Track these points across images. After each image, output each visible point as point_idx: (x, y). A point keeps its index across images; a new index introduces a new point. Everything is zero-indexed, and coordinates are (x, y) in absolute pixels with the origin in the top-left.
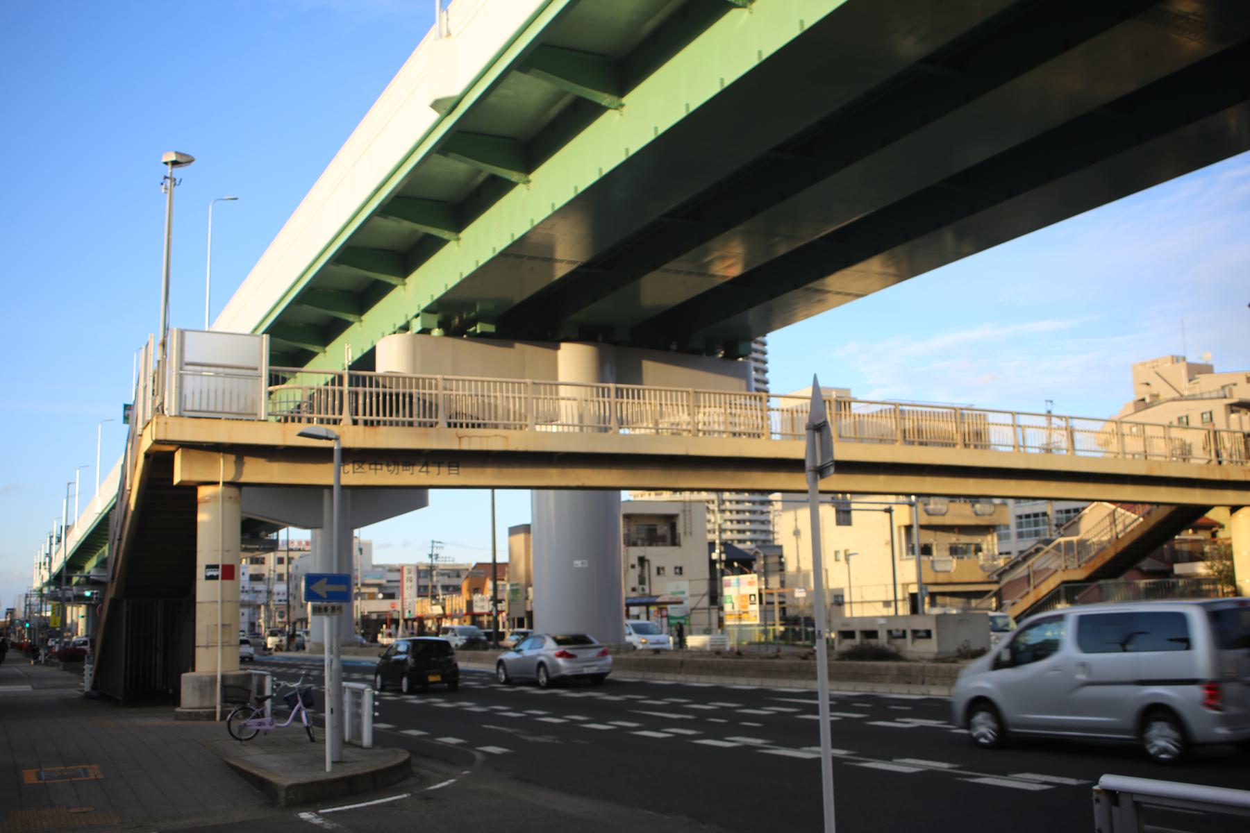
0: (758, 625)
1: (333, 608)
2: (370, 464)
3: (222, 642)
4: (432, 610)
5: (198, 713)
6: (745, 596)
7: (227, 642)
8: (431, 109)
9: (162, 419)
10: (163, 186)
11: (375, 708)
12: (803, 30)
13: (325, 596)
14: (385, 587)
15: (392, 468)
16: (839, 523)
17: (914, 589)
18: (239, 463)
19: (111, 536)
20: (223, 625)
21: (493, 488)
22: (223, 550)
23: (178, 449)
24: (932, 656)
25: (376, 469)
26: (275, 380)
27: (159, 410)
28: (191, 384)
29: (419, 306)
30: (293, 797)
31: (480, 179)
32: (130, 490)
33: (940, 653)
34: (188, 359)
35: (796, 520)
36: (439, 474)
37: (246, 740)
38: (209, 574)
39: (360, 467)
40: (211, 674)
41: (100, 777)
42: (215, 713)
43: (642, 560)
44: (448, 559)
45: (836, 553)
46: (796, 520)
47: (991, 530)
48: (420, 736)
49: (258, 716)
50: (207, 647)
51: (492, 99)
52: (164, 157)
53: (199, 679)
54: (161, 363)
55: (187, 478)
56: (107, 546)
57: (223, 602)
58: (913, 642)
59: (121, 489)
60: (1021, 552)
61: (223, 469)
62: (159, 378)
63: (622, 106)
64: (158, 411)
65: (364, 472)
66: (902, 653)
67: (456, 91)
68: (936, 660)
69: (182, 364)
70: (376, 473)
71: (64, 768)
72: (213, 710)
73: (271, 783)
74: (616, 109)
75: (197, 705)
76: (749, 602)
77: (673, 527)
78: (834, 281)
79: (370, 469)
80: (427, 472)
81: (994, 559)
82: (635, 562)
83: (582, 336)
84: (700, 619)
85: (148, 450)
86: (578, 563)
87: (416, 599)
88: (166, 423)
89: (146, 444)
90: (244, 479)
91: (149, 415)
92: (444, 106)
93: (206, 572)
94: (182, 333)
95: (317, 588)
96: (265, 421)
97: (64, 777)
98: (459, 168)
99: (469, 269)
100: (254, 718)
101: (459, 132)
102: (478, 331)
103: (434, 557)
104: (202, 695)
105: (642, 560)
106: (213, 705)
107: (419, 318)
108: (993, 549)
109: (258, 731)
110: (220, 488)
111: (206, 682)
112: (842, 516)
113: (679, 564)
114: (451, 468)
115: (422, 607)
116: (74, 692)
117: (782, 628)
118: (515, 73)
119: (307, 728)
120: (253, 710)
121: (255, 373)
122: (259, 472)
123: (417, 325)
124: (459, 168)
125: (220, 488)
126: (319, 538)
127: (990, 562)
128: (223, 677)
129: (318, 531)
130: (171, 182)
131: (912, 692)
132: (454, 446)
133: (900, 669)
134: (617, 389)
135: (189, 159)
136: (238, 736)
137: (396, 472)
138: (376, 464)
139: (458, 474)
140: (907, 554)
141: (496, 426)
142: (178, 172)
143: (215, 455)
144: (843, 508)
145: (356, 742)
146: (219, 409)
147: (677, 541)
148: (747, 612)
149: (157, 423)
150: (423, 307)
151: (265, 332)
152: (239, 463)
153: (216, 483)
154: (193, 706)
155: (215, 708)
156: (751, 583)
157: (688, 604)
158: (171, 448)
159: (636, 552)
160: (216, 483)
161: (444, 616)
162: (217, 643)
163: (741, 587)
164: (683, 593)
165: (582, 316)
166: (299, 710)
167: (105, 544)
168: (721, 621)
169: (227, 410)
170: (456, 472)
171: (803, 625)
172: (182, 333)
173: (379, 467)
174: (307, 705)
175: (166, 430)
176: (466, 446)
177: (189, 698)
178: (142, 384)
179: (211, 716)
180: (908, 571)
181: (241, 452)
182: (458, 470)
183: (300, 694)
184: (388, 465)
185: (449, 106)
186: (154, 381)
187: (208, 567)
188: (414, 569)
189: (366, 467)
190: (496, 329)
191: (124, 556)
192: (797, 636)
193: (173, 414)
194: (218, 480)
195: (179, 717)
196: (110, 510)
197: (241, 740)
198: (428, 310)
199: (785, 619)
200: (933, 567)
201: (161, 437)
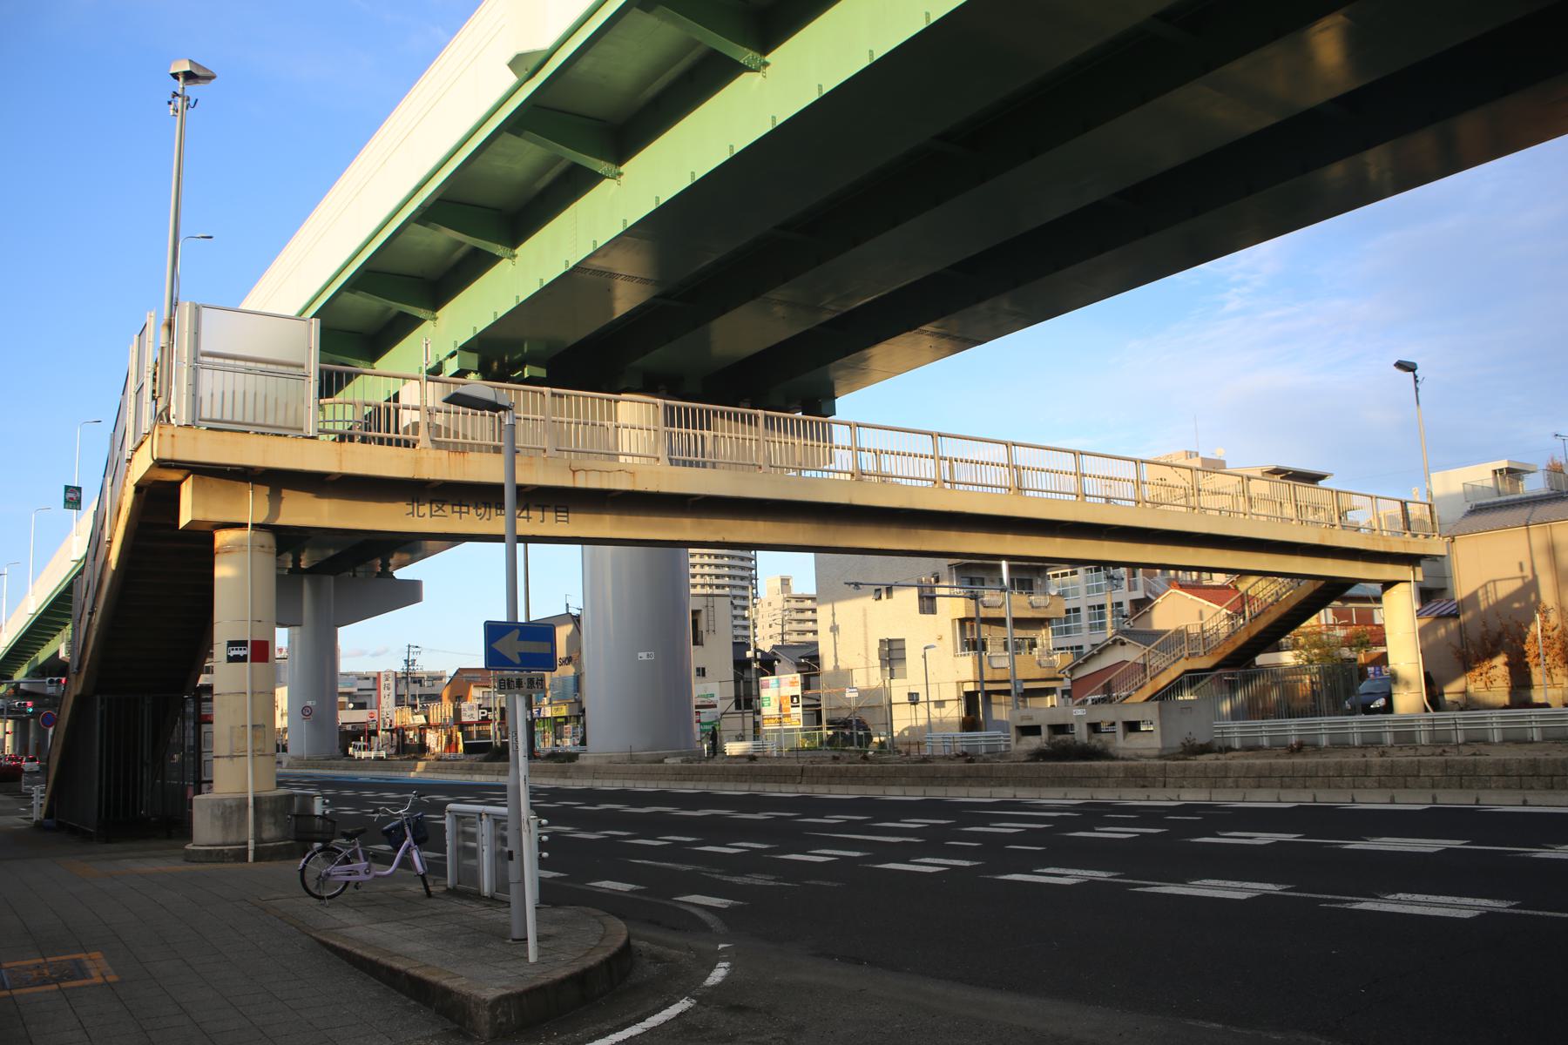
0: (801, 730)
1: (531, 681)
2: (453, 505)
3: (253, 751)
4: (413, 719)
5: (222, 850)
6: (786, 697)
7: (259, 750)
8: (508, 67)
9: (168, 431)
10: (172, 107)
11: (542, 846)
12: (821, 95)
13: (518, 661)
14: (356, 696)
15: (481, 511)
16: (922, 611)
17: (970, 687)
18: (275, 499)
19: (76, 611)
20: (254, 726)
22: (252, 621)
23: (186, 477)
24: (1156, 752)
25: (460, 512)
26: (330, 384)
27: (162, 417)
28: (211, 382)
29: (456, 342)
30: (504, 1020)
31: (463, 250)
32: (110, 542)
33: (1163, 749)
34: (204, 347)
35: (834, 615)
36: (542, 521)
37: (329, 898)
38: (232, 654)
39: (440, 509)
40: (238, 796)
41: (112, 978)
42: (246, 851)
46: (834, 615)
47: (1047, 623)
48: (554, 878)
49: (347, 861)
50: (231, 757)
51: (584, 65)
52: (172, 66)
53: (220, 803)
54: (166, 350)
55: (200, 517)
56: (69, 627)
57: (253, 693)
58: (1125, 736)
59: (93, 545)
60: (1094, 646)
61: (252, 506)
62: (161, 373)
63: (620, 174)
64: (162, 419)
66: (1111, 750)
67: (546, 44)
68: (1160, 757)
69: (198, 355)
70: (461, 518)
71: (42, 961)
72: (244, 847)
73: (447, 992)
74: (614, 178)
75: (219, 840)
76: (791, 704)
78: (879, 353)
79: (453, 512)
80: (528, 518)
81: (1049, 655)
83: (649, 386)
84: (733, 723)
85: (142, 479)
86: (643, 655)
87: (395, 708)
88: (173, 436)
89: (141, 466)
90: (281, 521)
91: (147, 423)
92: (525, 65)
93: (228, 651)
94: (197, 309)
95: (504, 645)
96: (312, 438)
97: (45, 983)
98: (442, 238)
99: (506, 306)
100: (340, 864)
101: (367, 271)
102: (526, 375)
104: (226, 826)
106: (243, 839)
107: (456, 357)
108: (1048, 644)
109: (347, 883)
110: (248, 532)
111: (231, 807)
112: (926, 602)
114: (558, 514)
115: (402, 717)
116: (15, 821)
117: (830, 733)
118: (506, 135)
119: (423, 877)
120: (340, 852)
121: (300, 371)
122: (302, 511)
123: (452, 366)
124: (442, 238)
125: (248, 532)
126: (297, 638)
127: (1045, 658)
128: (256, 799)
129: (297, 630)
130: (183, 100)
131: (1357, 800)
132: (566, 481)
133: (1126, 769)
134: (766, 417)
135: (209, 74)
136: (317, 893)
137: (487, 516)
138: (460, 505)
139: (568, 521)
140: (963, 650)
142: (193, 90)
143: (241, 485)
144: (927, 592)
145: (500, 895)
146: (249, 419)
147: (699, 639)
148: (789, 716)
149: (160, 435)
150: (459, 344)
151: (315, 316)
152: (275, 499)
153: (242, 526)
154: (212, 843)
155: (246, 843)
156: (793, 684)
157: (721, 708)
158: (174, 476)
160: (242, 526)
161: (428, 725)
162: (246, 751)
163: (782, 688)
164: (712, 696)
165: (659, 357)
166: (407, 851)
167: (66, 624)
168: (756, 725)
169: (260, 421)
170: (565, 519)
171: (855, 728)
172: (197, 309)
173: (464, 509)
174: (420, 841)
175: (173, 445)
177: (206, 830)
178: (132, 386)
179: (241, 856)
180: (965, 668)
181: (278, 481)
182: (567, 516)
183: (409, 825)
184: (477, 507)
185: (532, 66)
186: (154, 380)
187: (232, 644)
188: (391, 675)
189: (448, 508)
190: (547, 374)
191: (97, 635)
192: (848, 740)
193: (184, 423)
194: (244, 521)
195: (191, 857)
196: (76, 577)
197: (321, 898)
198: (467, 347)
199: (832, 723)
200: (990, 663)
201: (166, 455)
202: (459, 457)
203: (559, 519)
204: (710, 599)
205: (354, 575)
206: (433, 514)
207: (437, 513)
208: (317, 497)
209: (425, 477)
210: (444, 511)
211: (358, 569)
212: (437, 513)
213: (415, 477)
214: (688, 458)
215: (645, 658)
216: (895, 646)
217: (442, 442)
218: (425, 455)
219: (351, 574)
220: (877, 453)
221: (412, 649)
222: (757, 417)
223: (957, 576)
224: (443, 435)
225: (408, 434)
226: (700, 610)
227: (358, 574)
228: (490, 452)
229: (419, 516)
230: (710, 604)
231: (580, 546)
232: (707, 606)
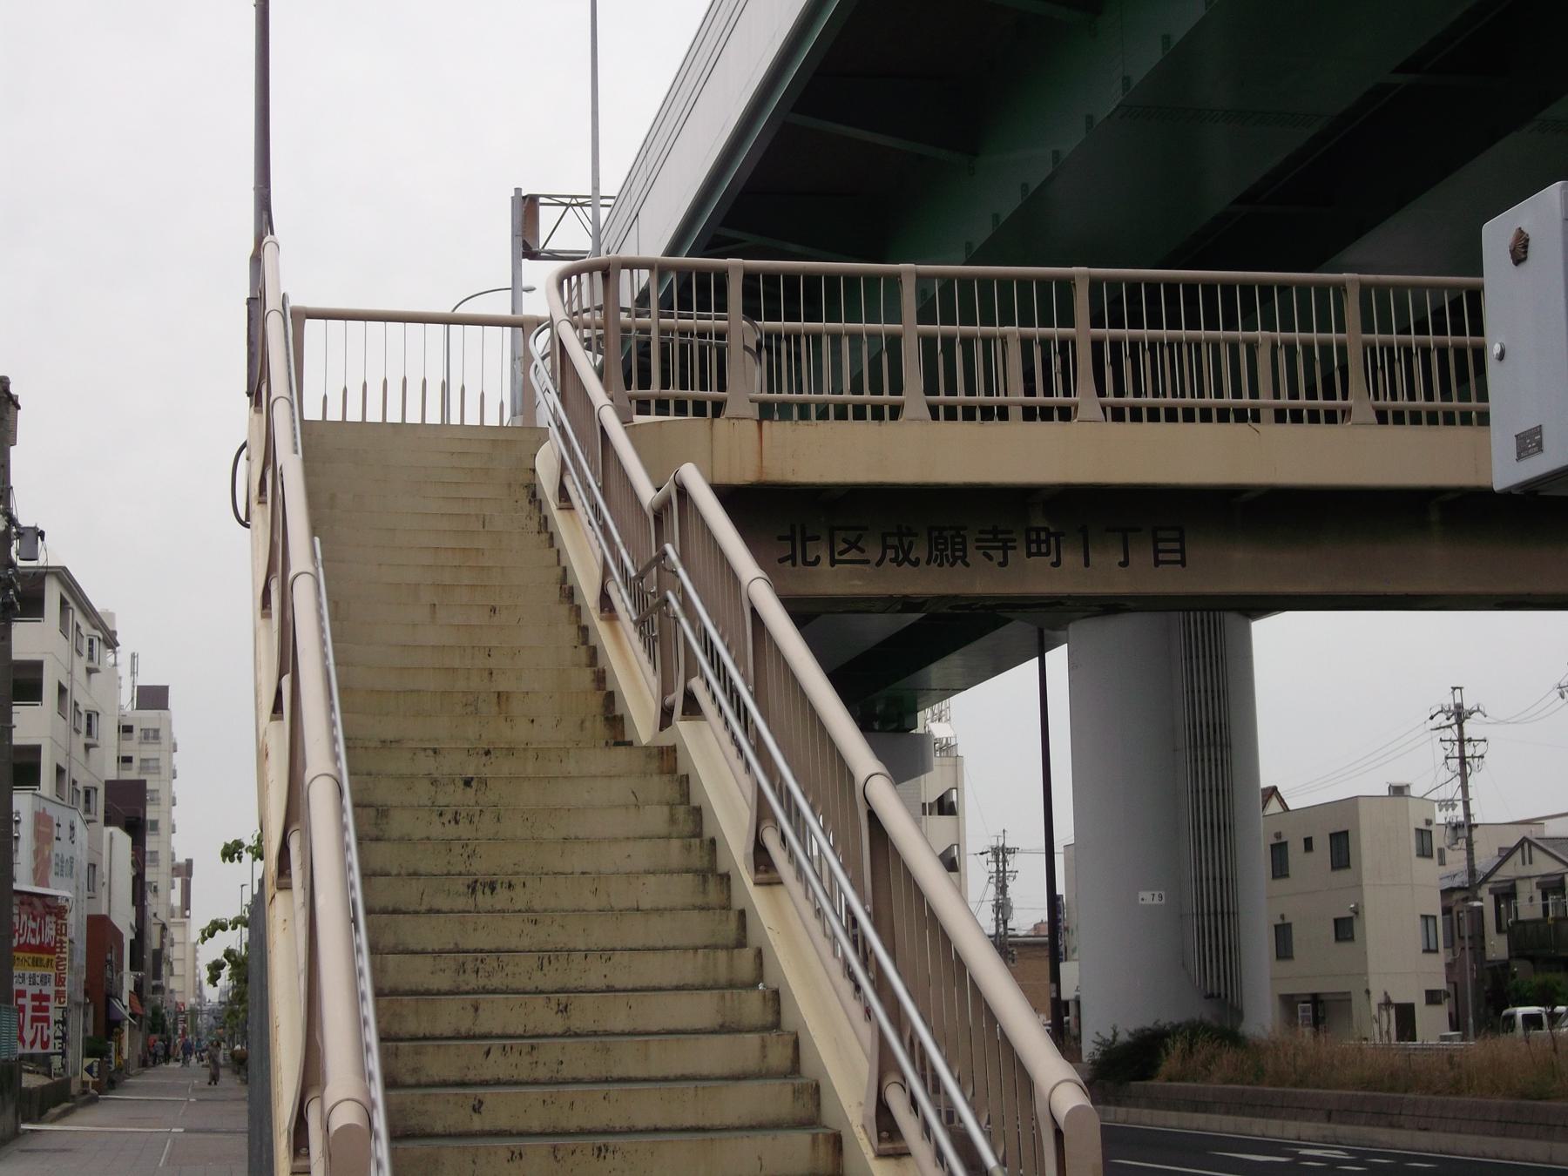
39: (853, 545)
139: (1183, 563)
170: (1177, 557)
203: (1161, 557)
206: (837, 557)
207: (845, 557)
208: (1142, 1030)
210: (862, 551)
212: (845, 557)
214: (1389, 403)
222: (1066, 285)
229: (805, 563)
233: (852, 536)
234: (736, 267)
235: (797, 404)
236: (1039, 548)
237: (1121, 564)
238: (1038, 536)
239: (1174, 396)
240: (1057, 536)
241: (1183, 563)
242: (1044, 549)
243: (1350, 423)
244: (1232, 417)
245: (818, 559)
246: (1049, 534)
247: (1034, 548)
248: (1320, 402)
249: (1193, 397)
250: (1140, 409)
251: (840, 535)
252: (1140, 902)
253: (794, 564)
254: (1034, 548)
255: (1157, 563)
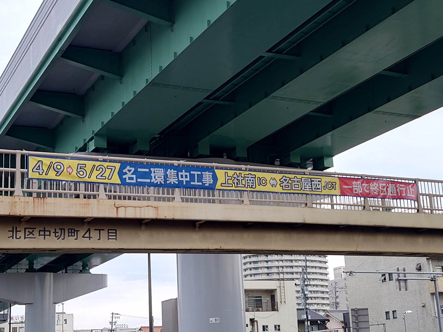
21: (149, 251)
25: (45, 235)
36: (99, 239)
39: (31, 233)
43: (252, 321)
44: (123, 326)
45: (387, 313)
65: (35, 238)
70: (45, 239)
77: (273, 298)
79: (40, 235)
82: (248, 322)
103: (113, 324)
105: (252, 321)
113: (277, 324)
132: (112, 214)
137: (62, 237)
139: (116, 239)
141: (149, 199)
159: (249, 315)
170: (115, 237)
176: (122, 214)
202: (41, 201)
203: (110, 237)
204: (282, 282)
205: (66, 272)
206: (26, 236)
207: (28, 236)
209: (18, 214)
210: (34, 235)
211: (68, 268)
212: (28, 236)
213: (11, 214)
214: (142, 195)
215: (214, 322)
216: (361, 313)
217: (254, 201)
218: (18, 200)
219: (64, 271)
220: (431, 196)
221: (114, 316)
222: (14, 156)
223: (432, 265)
224: (268, 198)
225: (8, 187)
226: (276, 289)
227: (68, 271)
228: (206, 203)
230: (282, 285)
231: (176, 254)
232: (280, 287)
233: (31, 230)
234: (18, 153)
235: (74, 194)
236: (71, 234)
237: (98, 239)
238: (71, 231)
239: (131, 193)
240: (77, 231)
241: (116, 239)
242: (73, 234)
243: (243, 204)
244: (162, 200)
245: (20, 237)
246: (75, 231)
247: (70, 234)
248: (9, 189)
249: (136, 193)
250: (116, 196)
251: (27, 230)
252: (210, 322)
253: (13, 238)
254: (70, 234)
255: (109, 239)
